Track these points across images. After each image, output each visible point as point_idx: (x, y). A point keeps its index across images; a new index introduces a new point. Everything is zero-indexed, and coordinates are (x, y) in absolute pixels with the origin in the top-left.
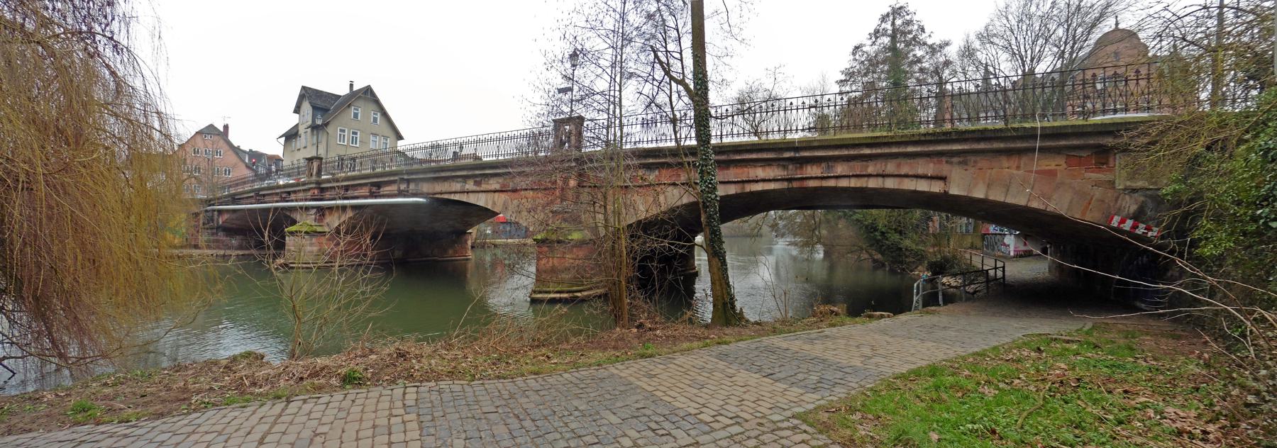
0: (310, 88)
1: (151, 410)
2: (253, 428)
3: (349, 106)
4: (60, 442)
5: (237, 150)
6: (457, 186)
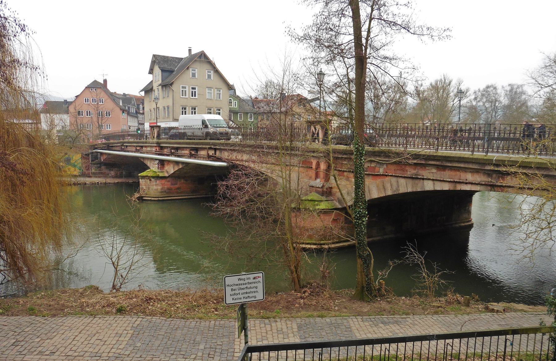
0: (159, 56)
1: (52, 313)
2: (79, 327)
3: (188, 68)
4: (27, 322)
5: (113, 96)
6: (245, 157)
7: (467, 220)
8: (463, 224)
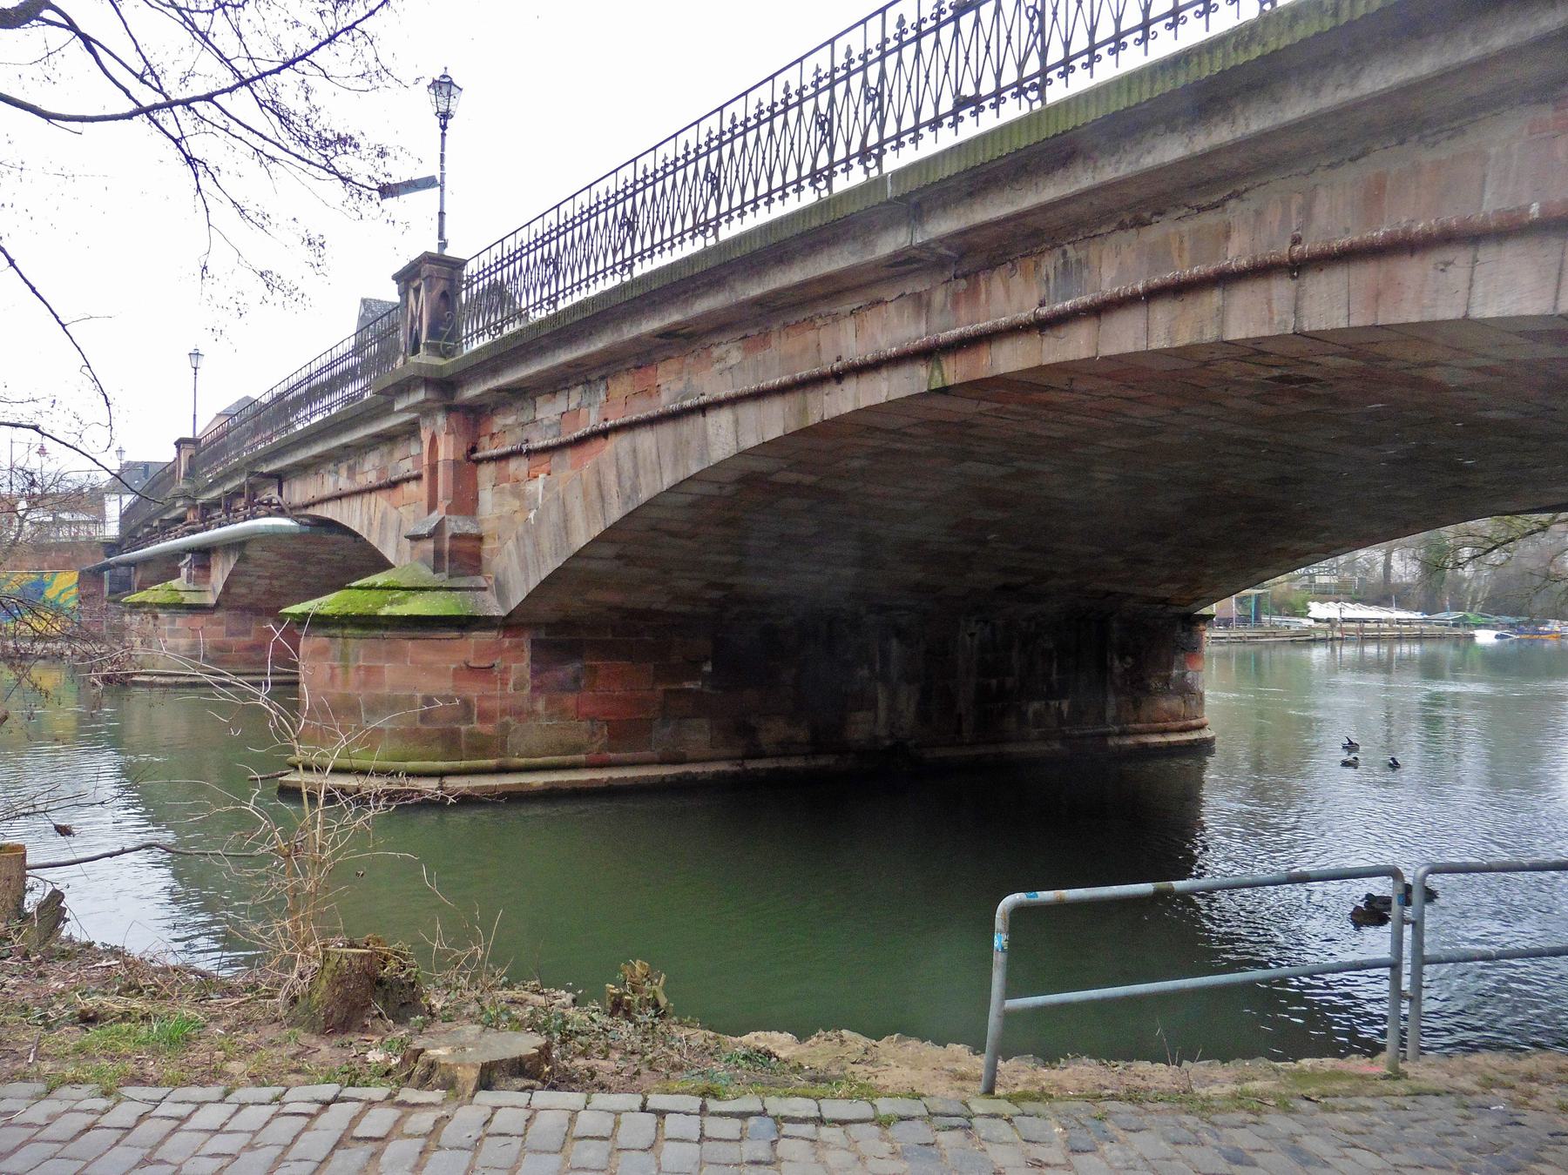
0: (379, 301)
7: (1180, 724)
8: (1156, 739)
